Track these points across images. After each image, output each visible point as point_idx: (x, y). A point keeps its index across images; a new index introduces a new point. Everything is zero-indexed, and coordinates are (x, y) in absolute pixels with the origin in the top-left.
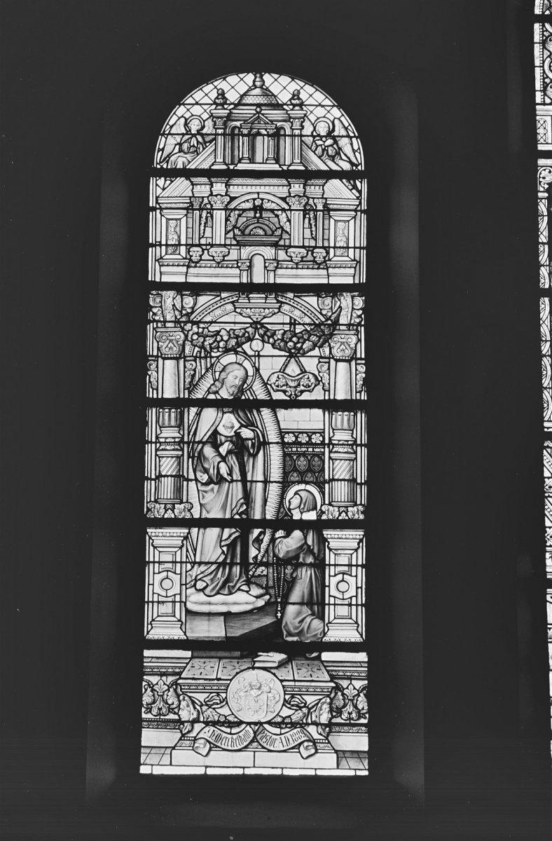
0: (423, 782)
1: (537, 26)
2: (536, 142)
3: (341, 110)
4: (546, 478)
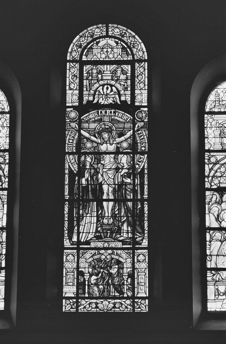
0: (197, 75)
1: (68, 64)
2: (66, 103)
3: (2, 92)
4: (65, 214)
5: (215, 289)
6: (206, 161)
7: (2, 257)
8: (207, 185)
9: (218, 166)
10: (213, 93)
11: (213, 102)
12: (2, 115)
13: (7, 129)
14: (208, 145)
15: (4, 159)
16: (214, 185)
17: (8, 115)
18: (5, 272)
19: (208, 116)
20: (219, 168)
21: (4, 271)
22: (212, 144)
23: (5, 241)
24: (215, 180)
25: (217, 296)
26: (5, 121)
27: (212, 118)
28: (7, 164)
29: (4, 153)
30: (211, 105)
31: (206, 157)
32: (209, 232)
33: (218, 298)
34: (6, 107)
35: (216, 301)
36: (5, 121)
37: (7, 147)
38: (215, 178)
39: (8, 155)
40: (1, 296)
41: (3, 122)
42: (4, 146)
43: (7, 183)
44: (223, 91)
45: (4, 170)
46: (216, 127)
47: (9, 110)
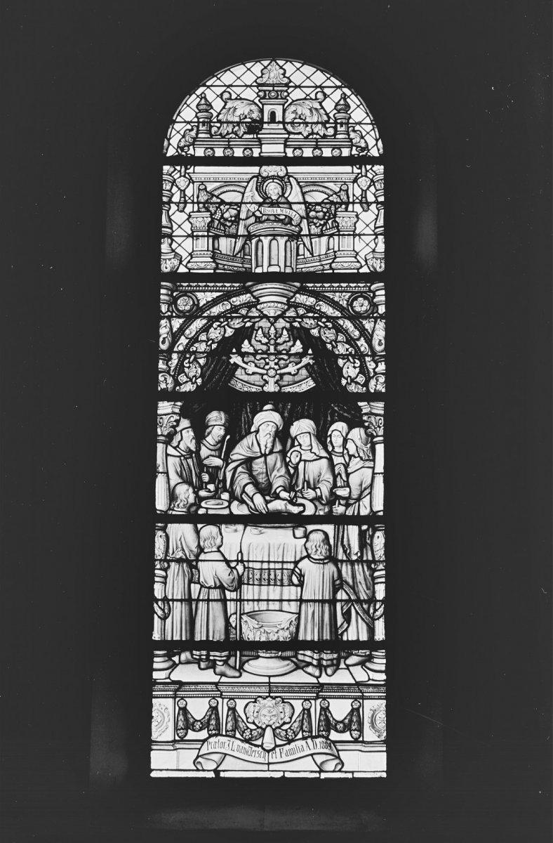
3: (359, 97)
5: (177, 708)
6: (164, 308)
7: (375, 610)
8: (165, 383)
9: (199, 323)
10: (193, 100)
11: (189, 127)
12: (360, 168)
13: (376, 212)
14: (170, 259)
15: (369, 303)
16: (187, 382)
17: (379, 169)
18: (387, 657)
19: (172, 169)
20: (206, 329)
21: (382, 653)
22: (184, 255)
23: (383, 558)
24: (189, 367)
25: (181, 733)
26: (370, 186)
27: (187, 176)
28: (381, 317)
29: (369, 285)
30: (184, 136)
31: (162, 297)
32: (164, 529)
33: (185, 736)
34: (371, 142)
35: (178, 746)
36: (370, 186)
37: (380, 266)
38: (191, 360)
39: (383, 292)
40: (377, 734)
41: (365, 189)
42: (370, 263)
43: (382, 379)
44: (222, 94)
45: (372, 336)
46: (198, 203)
47: (381, 151)
